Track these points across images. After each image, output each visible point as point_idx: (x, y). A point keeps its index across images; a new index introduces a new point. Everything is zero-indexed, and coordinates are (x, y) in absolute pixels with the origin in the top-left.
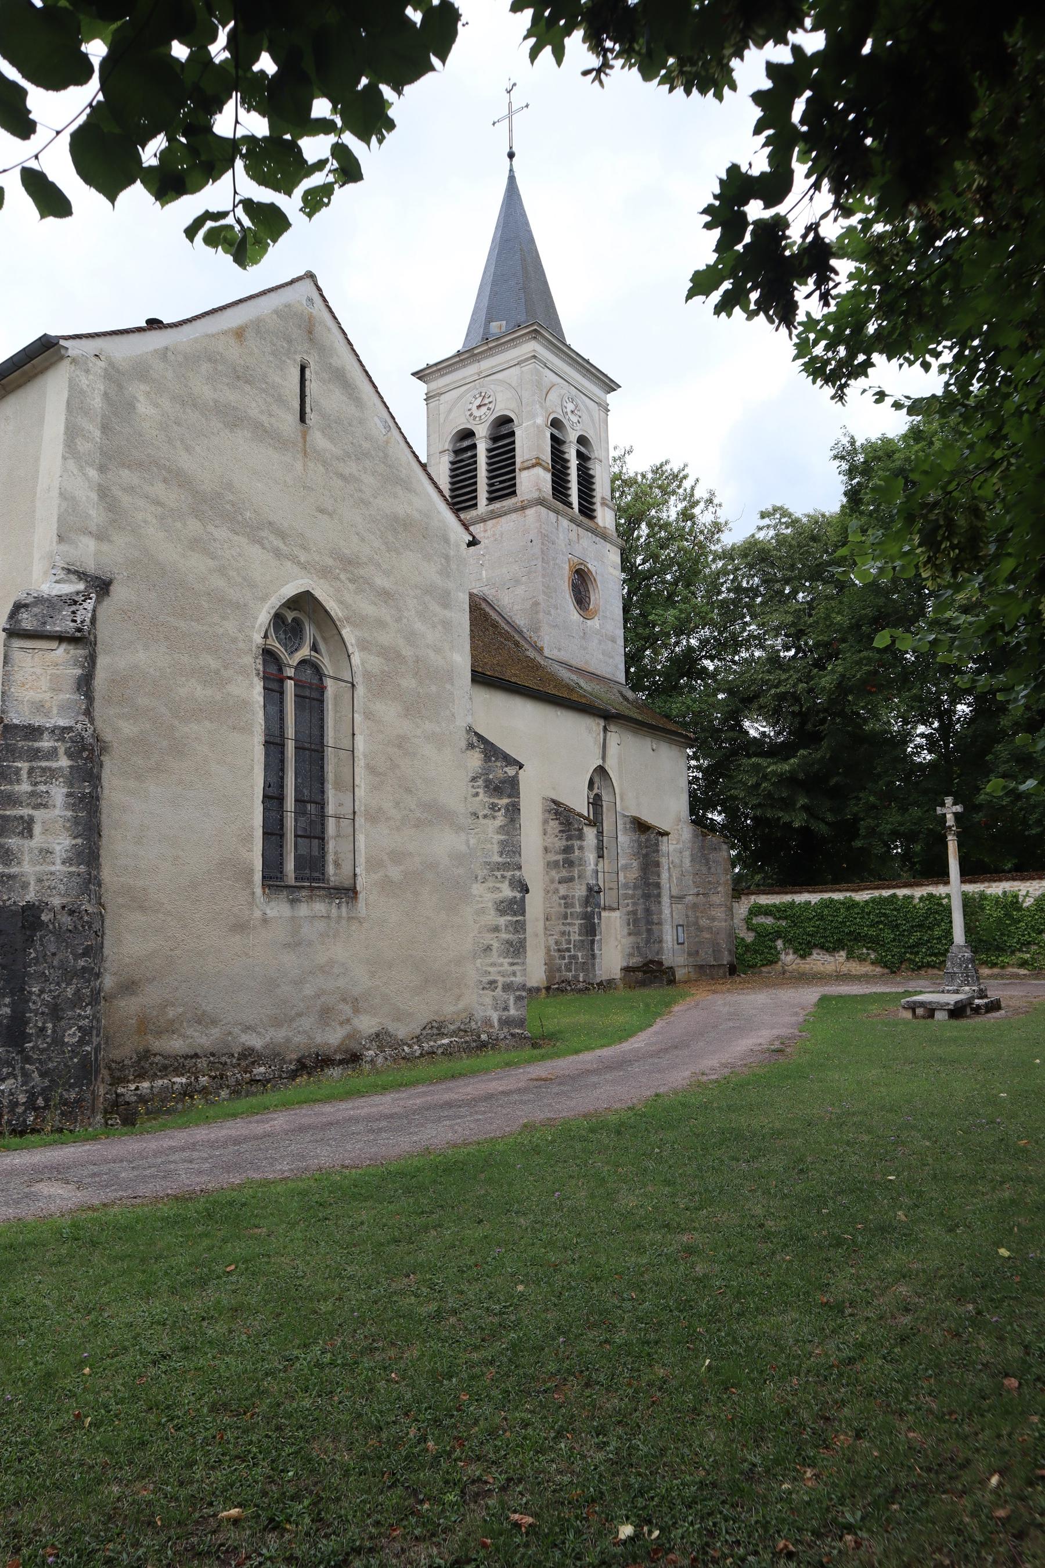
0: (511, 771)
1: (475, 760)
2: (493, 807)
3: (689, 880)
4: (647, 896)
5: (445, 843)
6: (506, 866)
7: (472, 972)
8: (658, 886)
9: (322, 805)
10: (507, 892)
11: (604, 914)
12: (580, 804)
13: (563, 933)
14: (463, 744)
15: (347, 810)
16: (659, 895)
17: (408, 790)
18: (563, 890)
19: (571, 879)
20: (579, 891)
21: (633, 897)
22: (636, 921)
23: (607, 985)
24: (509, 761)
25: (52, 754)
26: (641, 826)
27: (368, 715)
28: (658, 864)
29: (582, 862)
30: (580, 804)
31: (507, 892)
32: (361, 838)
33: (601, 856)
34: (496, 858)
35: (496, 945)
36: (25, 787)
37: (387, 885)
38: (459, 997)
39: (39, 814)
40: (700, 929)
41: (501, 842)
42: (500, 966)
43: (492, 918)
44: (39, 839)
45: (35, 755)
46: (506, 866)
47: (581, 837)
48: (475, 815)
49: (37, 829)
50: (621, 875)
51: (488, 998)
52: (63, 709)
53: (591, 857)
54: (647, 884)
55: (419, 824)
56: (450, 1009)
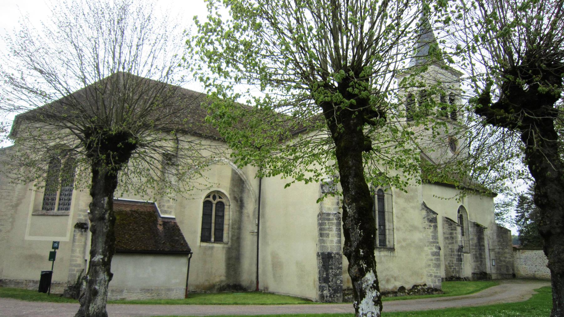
0: (434, 216)
1: (424, 213)
2: (430, 226)
3: (496, 243)
4: (480, 249)
5: (417, 236)
6: (434, 242)
7: (425, 271)
8: (484, 246)
9: (384, 226)
10: (435, 250)
11: (465, 255)
12: (456, 219)
13: (450, 261)
14: (421, 208)
15: (391, 228)
16: (484, 249)
17: (407, 222)
18: (450, 246)
19: (453, 243)
20: (456, 247)
21: (475, 249)
22: (476, 258)
23: (466, 279)
24: (434, 213)
25: (332, 219)
26: (477, 226)
27: (396, 203)
28: (483, 239)
29: (456, 237)
30: (456, 219)
31: (435, 250)
32: (395, 235)
33: (463, 235)
34: (431, 240)
35: (432, 264)
36: (327, 227)
37: (402, 247)
38: (422, 278)
39: (330, 233)
40: (501, 261)
41: (432, 236)
42: (433, 271)
43: (430, 257)
44: (330, 238)
45: (329, 220)
46: (434, 242)
47: (455, 230)
48: (425, 228)
49: (330, 236)
50: (471, 242)
51: (430, 279)
52: (334, 209)
53: (459, 236)
54: (480, 245)
55: (410, 231)
56: (419, 282)
